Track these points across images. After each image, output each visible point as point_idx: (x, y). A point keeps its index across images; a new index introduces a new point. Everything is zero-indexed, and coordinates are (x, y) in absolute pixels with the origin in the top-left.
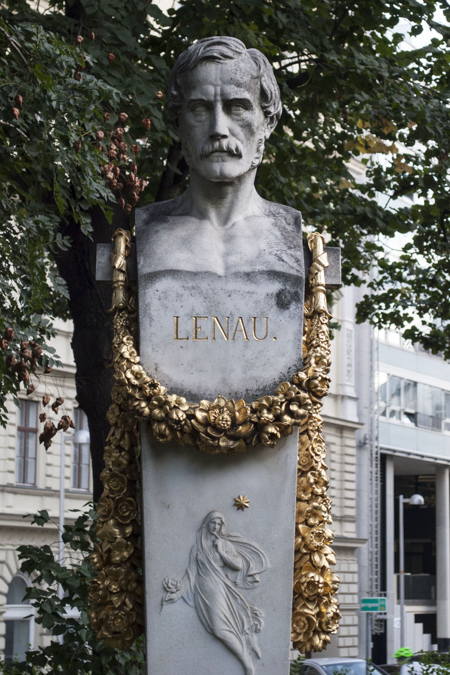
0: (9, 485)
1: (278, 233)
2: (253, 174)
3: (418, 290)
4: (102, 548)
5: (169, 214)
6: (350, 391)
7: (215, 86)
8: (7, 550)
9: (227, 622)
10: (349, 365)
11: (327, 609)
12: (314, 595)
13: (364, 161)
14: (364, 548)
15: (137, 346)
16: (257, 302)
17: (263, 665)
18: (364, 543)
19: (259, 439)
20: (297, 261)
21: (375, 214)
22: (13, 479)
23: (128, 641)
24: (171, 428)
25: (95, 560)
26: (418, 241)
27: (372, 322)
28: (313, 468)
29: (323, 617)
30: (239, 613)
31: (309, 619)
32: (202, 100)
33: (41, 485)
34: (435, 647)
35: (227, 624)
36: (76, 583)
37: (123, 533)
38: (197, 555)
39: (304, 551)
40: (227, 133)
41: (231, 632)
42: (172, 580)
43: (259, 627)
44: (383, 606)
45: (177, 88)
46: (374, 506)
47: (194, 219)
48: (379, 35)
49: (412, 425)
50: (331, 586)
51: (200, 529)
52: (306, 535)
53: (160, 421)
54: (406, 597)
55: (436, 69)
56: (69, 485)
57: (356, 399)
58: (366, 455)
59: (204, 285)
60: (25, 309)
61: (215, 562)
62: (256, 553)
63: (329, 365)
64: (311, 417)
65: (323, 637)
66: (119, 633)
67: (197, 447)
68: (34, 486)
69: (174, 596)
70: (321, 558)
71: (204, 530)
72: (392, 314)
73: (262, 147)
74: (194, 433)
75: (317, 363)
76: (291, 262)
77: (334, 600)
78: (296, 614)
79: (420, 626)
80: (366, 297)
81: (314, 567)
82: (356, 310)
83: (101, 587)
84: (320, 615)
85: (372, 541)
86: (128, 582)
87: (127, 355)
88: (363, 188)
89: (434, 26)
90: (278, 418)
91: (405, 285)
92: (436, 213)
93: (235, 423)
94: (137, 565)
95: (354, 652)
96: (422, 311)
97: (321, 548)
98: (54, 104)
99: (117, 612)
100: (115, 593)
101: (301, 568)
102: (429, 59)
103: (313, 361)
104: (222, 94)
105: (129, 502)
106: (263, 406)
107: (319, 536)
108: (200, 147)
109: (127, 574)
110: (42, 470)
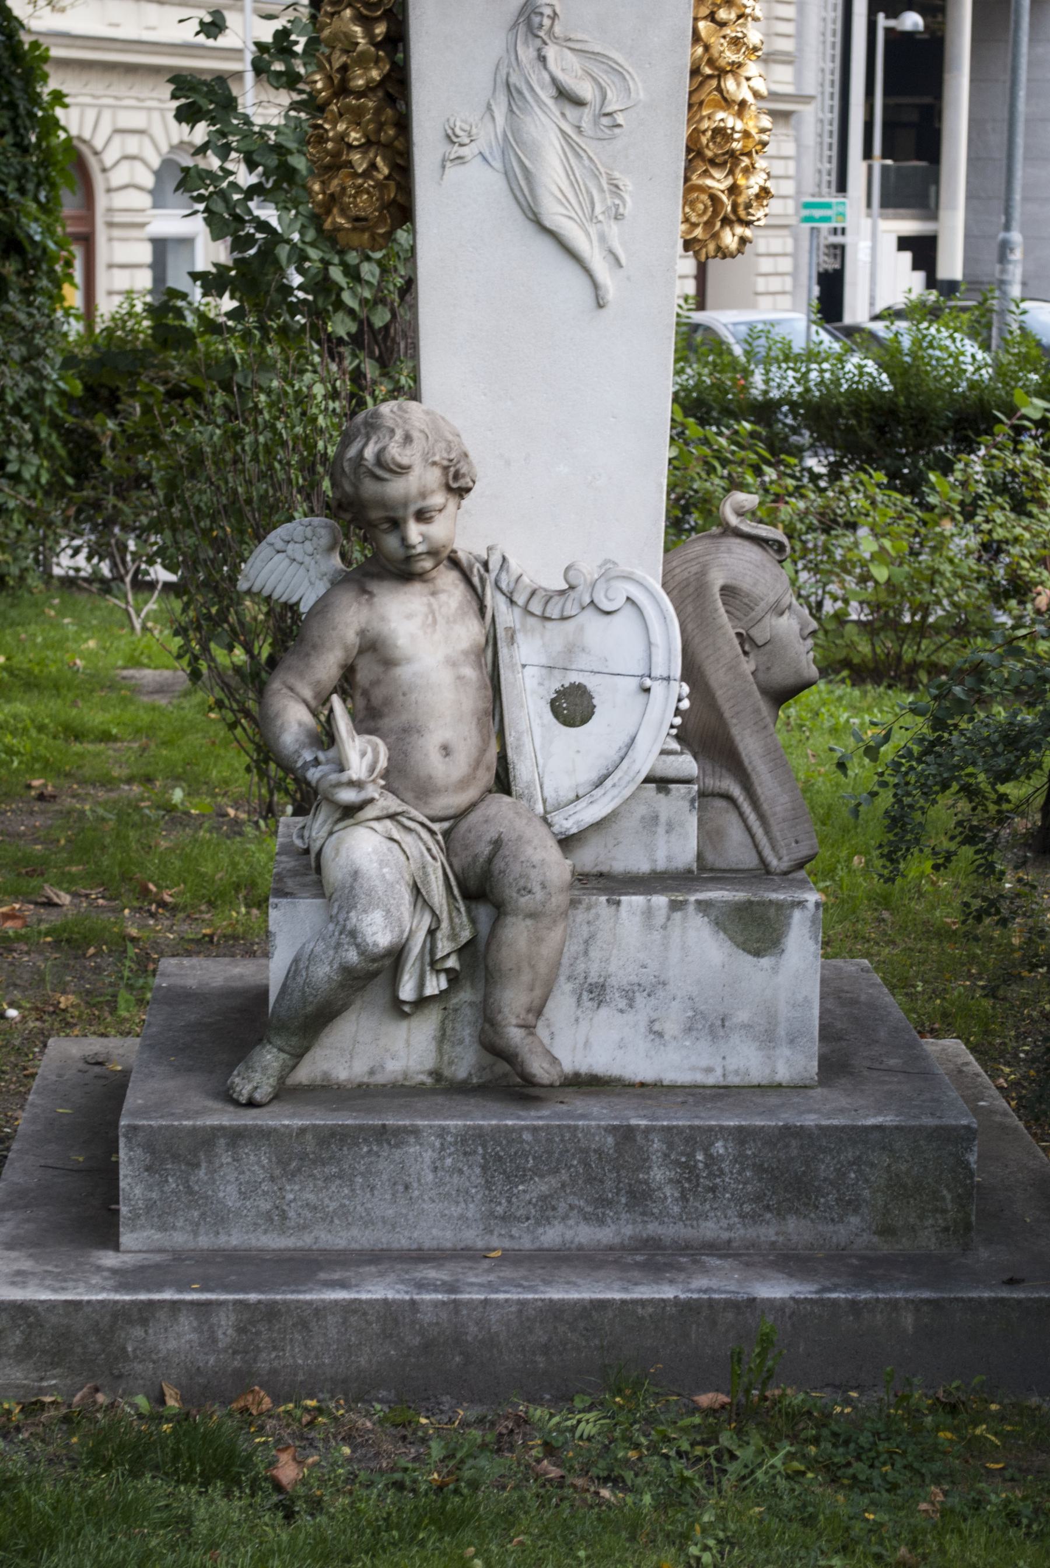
4: (330, 63)
8: (149, 109)
9: (564, 200)
11: (747, 178)
12: (724, 154)
17: (628, 279)
18: (808, 103)
23: (382, 235)
25: (319, 85)
29: (740, 194)
30: (585, 185)
31: (714, 198)
35: (562, 204)
37: (369, 34)
38: (508, 75)
39: (708, 71)
41: (570, 218)
42: (462, 121)
43: (621, 210)
44: (842, 215)
46: (829, 33)
50: (757, 137)
51: (515, 25)
52: (712, 40)
54: (885, 204)
61: (542, 88)
62: (618, 72)
65: (739, 230)
66: (365, 219)
70: (738, 85)
71: (522, 29)
77: (761, 163)
78: (690, 188)
79: (907, 257)
81: (726, 102)
83: (331, 134)
85: (823, 100)
86: (381, 127)
94: (397, 95)
95: (786, 301)
97: (740, 65)
99: (360, 181)
100: (357, 147)
101: (701, 103)
107: (736, 42)
109: (378, 111)
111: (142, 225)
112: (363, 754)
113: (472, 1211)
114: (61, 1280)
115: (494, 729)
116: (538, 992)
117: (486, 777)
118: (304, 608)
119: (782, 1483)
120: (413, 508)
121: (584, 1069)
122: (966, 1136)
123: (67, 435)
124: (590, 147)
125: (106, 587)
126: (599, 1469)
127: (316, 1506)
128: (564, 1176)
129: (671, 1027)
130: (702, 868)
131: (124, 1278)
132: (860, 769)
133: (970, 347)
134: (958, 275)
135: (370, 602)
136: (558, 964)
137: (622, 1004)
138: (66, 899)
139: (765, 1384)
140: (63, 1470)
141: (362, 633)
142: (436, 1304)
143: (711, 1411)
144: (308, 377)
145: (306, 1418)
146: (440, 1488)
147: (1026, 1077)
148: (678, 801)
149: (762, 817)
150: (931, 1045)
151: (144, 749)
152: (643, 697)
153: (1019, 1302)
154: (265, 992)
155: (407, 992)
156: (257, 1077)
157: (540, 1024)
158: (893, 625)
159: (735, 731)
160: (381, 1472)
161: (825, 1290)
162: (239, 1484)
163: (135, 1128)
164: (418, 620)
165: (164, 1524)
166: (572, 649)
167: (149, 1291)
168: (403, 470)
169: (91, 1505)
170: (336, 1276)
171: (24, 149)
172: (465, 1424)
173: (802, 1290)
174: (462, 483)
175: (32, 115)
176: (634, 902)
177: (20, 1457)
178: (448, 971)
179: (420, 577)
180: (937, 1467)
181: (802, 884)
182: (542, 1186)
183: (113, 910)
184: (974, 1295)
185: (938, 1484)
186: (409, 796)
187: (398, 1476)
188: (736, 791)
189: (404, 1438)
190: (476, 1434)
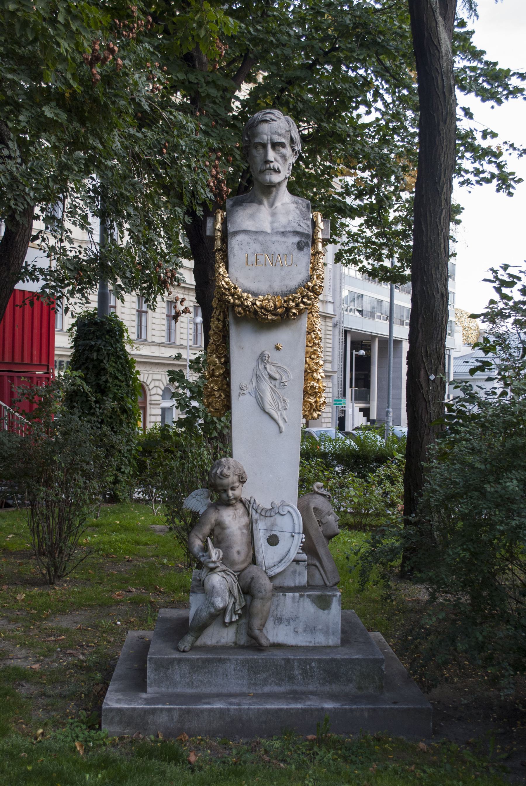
0: (163, 343)
1: (298, 212)
2: (286, 182)
3: (366, 247)
5: (243, 202)
6: (330, 299)
7: (267, 135)
10: (330, 286)
13: (340, 181)
14: (335, 376)
15: (227, 268)
16: (287, 247)
19: (288, 316)
20: (308, 226)
21: (346, 207)
22: (164, 340)
24: (244, 310)
26: (366, 222)
27: (342, 263)
28: (314, 331)
31: (311, 404)
32: (260, 143)
33: (178, 343)
34: (369, 423)
36: (196, 390)
37: (220, 361)
40: (273, 160)
45: (248, 136)
47: (256, 205)
48: (349, 115)
49: (360, 316)
51: (258, 359)
53: (238, 306)
55: (377, 133)
56: (191, 343)
57: (333, 303)
58: (337, 331)
59: (261, 238)
60: (169, 253)
62: (285, 371)
63: (323, 279)
64: (313, 305)
65: (318, 412)
67: (257, 319)
68: (175, 343)
69: (244, 392)
71: (260, 360)
72: (353, 259)
73: (291, 168)
74: (256, 312)
75: (317, 278)
76: (305, 226)
78: (304, 401)
79: (362, 413)
80: (340, 250)
81: (314, 379)
82: (335, 256)
84: (316, 402)
86: (223, 385)
87: (222, 273)
88: (339, 194)
89: (377, 109)
90: (297, 305)
91: (359, 244)
92: (376, 207)
93: (276, 308)
96: (367, 258)
98: (184, 148)
102: (374, 128)
103: (315, 277)
104: (271, 140)
105: (223, 346)
106: (289, 299)
107: (317, 364)
108: (259, 167)
109: (222, 381)
110: (178, 336)
111: (159, 404)
112: (216, 554)
113: (245, 682)
114: (130, 702)
115: (252, 547)
116: (263, 620)
117: (249, 560)
118: (200, 513)
119: (331, 762)
120: (230, 487)
121: (276, 642)
122: (381, 661)
123: (137, 460)
124: (278, 391)
125: (147, 502)
126: (280, 758)
127: (201, 768)
128: (270, 672)
129: (300, 630)
130: (308, 585)
131: (148, 701)
132: (352, 556)
133: (379, 438)
134: (375, 418)
135: (218, 512)
136: (269, 612)
137: (287, 623)
138: (134, 590)
139: (326, 733)
140: (130, 757)
141: (216, 520)
142: (234, 709)
143: (312, 740)
144: (202, 449)
145: (198, 742)
146: (235, 763)
147: (397, 642)
148: (301, 568)
149: (324, 571)
150: (371, 634)
151: (156, 548)
152: (292, 538)
153: (397, 709)
154: (187, 619)
155: (227, 620)
156: (186, 644)
157: (264, 629)
158: (360, 514)
159: (317, 547)
160: (219, 758)
161: (343, 705)
162: (179, 761)
163: (151, 658)
164: (231, 517)
165: (158, 774)
166: (273, 525)
167: (155, 705)
168: (227, 476)
169: (137, 768)
170: (207, 701)
171: (128, 386)
172: (243, 744)
173: (337, 705)
174: (243, 480)
175: (131, 377)
176: (290, 595)
177: (118, 753)
178: (238, 614)
179: (232, 505)
180: (375, 757)
181: (336, 590)
182: (264, 675)
183: (147, 593)
184: (384, 706)
185: (375, 762)
186: (228, 565)
187: (223, 759)
188: (318, 564)
189: (225, 748)
190: (245, 747)
